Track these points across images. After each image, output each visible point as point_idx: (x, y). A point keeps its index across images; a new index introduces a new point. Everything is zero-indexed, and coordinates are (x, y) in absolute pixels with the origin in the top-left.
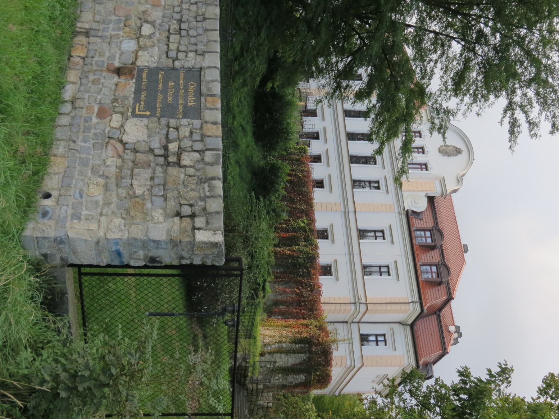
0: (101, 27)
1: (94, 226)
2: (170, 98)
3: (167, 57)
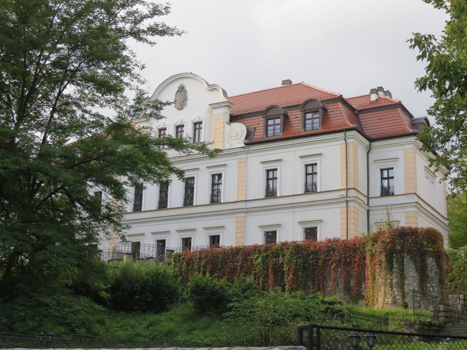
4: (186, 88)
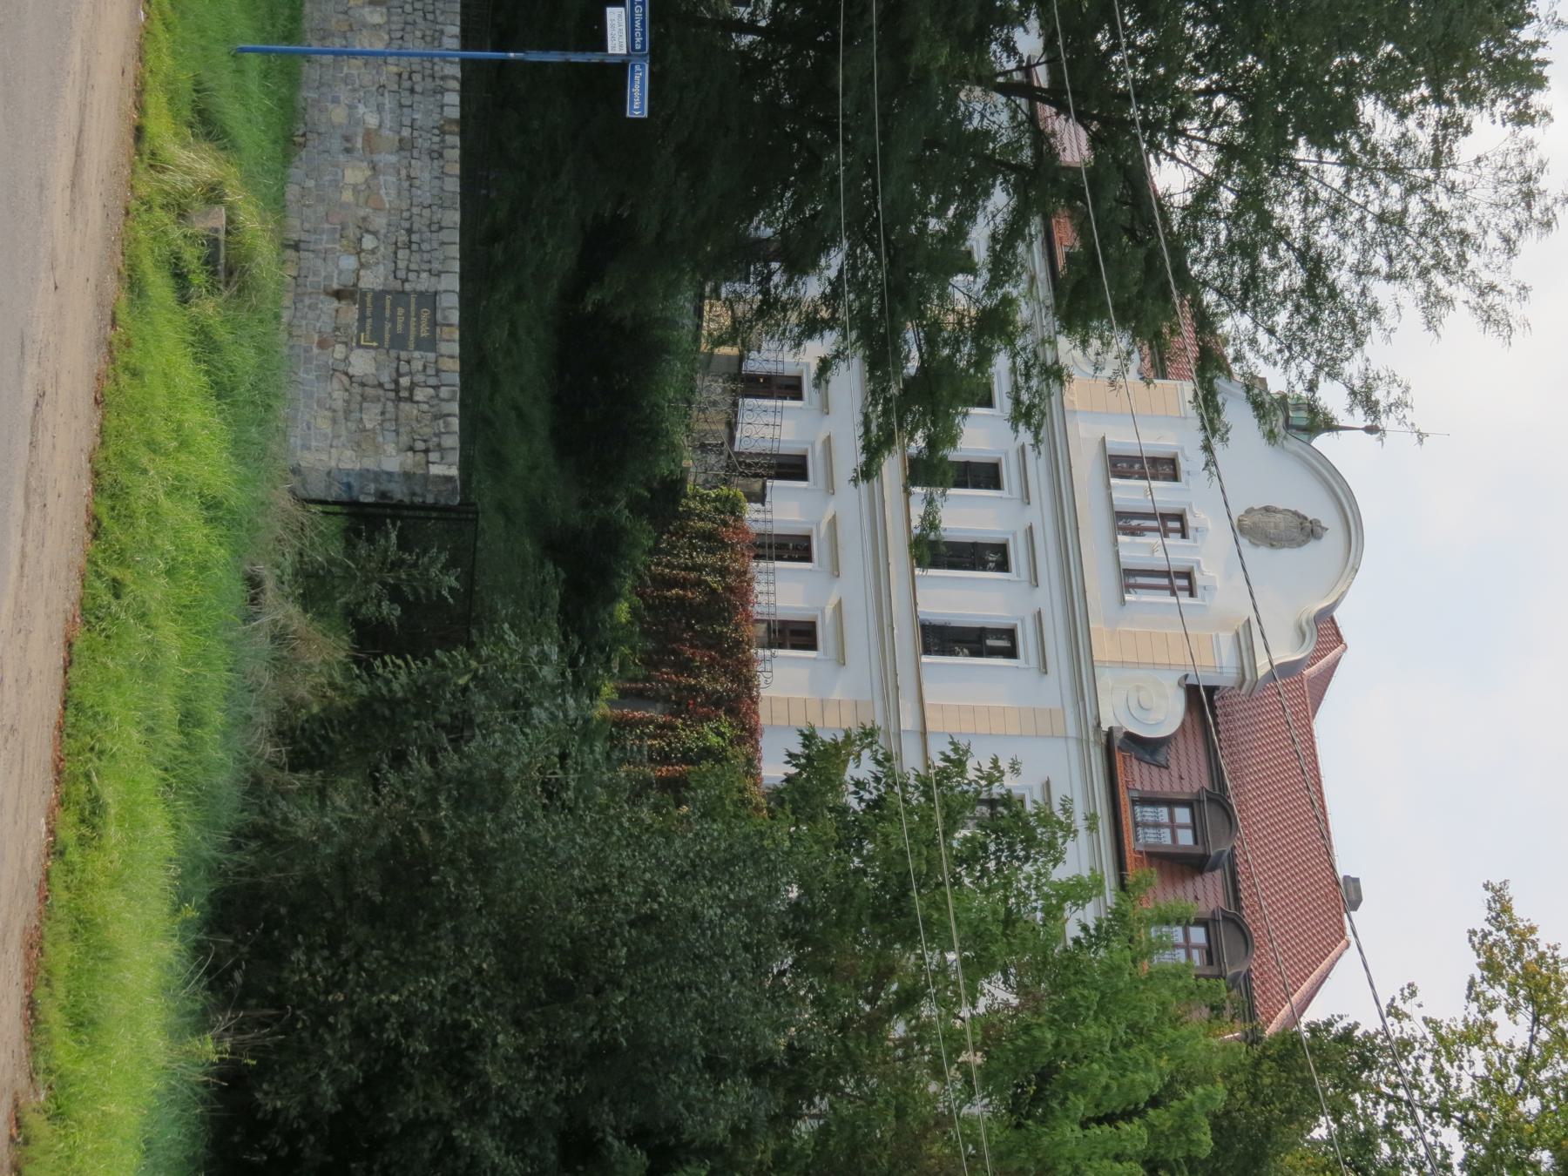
0: (313, 237)
1: (324, 457)
2: (400, 328)
3: (395, 277)
4: (1312, 546)
